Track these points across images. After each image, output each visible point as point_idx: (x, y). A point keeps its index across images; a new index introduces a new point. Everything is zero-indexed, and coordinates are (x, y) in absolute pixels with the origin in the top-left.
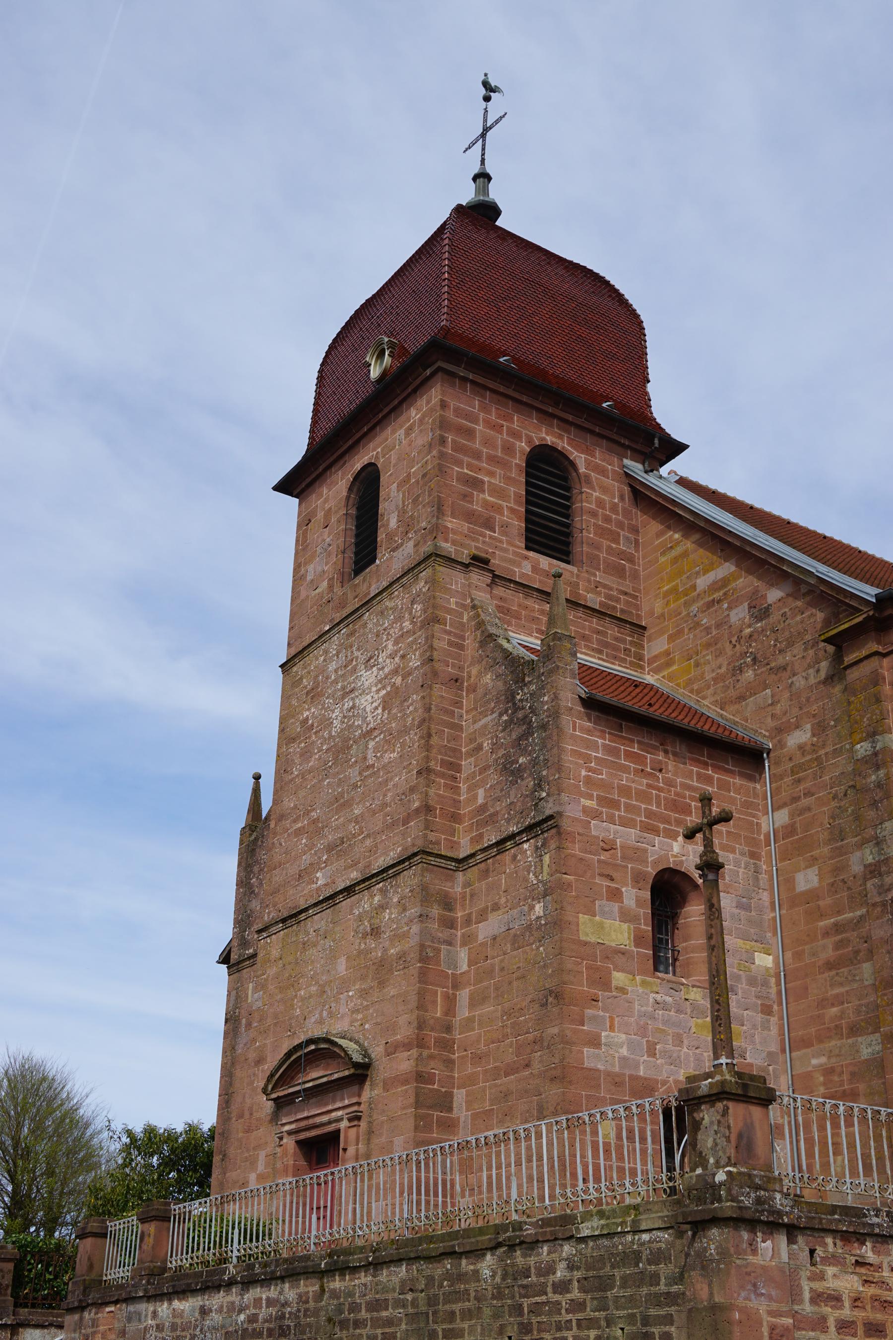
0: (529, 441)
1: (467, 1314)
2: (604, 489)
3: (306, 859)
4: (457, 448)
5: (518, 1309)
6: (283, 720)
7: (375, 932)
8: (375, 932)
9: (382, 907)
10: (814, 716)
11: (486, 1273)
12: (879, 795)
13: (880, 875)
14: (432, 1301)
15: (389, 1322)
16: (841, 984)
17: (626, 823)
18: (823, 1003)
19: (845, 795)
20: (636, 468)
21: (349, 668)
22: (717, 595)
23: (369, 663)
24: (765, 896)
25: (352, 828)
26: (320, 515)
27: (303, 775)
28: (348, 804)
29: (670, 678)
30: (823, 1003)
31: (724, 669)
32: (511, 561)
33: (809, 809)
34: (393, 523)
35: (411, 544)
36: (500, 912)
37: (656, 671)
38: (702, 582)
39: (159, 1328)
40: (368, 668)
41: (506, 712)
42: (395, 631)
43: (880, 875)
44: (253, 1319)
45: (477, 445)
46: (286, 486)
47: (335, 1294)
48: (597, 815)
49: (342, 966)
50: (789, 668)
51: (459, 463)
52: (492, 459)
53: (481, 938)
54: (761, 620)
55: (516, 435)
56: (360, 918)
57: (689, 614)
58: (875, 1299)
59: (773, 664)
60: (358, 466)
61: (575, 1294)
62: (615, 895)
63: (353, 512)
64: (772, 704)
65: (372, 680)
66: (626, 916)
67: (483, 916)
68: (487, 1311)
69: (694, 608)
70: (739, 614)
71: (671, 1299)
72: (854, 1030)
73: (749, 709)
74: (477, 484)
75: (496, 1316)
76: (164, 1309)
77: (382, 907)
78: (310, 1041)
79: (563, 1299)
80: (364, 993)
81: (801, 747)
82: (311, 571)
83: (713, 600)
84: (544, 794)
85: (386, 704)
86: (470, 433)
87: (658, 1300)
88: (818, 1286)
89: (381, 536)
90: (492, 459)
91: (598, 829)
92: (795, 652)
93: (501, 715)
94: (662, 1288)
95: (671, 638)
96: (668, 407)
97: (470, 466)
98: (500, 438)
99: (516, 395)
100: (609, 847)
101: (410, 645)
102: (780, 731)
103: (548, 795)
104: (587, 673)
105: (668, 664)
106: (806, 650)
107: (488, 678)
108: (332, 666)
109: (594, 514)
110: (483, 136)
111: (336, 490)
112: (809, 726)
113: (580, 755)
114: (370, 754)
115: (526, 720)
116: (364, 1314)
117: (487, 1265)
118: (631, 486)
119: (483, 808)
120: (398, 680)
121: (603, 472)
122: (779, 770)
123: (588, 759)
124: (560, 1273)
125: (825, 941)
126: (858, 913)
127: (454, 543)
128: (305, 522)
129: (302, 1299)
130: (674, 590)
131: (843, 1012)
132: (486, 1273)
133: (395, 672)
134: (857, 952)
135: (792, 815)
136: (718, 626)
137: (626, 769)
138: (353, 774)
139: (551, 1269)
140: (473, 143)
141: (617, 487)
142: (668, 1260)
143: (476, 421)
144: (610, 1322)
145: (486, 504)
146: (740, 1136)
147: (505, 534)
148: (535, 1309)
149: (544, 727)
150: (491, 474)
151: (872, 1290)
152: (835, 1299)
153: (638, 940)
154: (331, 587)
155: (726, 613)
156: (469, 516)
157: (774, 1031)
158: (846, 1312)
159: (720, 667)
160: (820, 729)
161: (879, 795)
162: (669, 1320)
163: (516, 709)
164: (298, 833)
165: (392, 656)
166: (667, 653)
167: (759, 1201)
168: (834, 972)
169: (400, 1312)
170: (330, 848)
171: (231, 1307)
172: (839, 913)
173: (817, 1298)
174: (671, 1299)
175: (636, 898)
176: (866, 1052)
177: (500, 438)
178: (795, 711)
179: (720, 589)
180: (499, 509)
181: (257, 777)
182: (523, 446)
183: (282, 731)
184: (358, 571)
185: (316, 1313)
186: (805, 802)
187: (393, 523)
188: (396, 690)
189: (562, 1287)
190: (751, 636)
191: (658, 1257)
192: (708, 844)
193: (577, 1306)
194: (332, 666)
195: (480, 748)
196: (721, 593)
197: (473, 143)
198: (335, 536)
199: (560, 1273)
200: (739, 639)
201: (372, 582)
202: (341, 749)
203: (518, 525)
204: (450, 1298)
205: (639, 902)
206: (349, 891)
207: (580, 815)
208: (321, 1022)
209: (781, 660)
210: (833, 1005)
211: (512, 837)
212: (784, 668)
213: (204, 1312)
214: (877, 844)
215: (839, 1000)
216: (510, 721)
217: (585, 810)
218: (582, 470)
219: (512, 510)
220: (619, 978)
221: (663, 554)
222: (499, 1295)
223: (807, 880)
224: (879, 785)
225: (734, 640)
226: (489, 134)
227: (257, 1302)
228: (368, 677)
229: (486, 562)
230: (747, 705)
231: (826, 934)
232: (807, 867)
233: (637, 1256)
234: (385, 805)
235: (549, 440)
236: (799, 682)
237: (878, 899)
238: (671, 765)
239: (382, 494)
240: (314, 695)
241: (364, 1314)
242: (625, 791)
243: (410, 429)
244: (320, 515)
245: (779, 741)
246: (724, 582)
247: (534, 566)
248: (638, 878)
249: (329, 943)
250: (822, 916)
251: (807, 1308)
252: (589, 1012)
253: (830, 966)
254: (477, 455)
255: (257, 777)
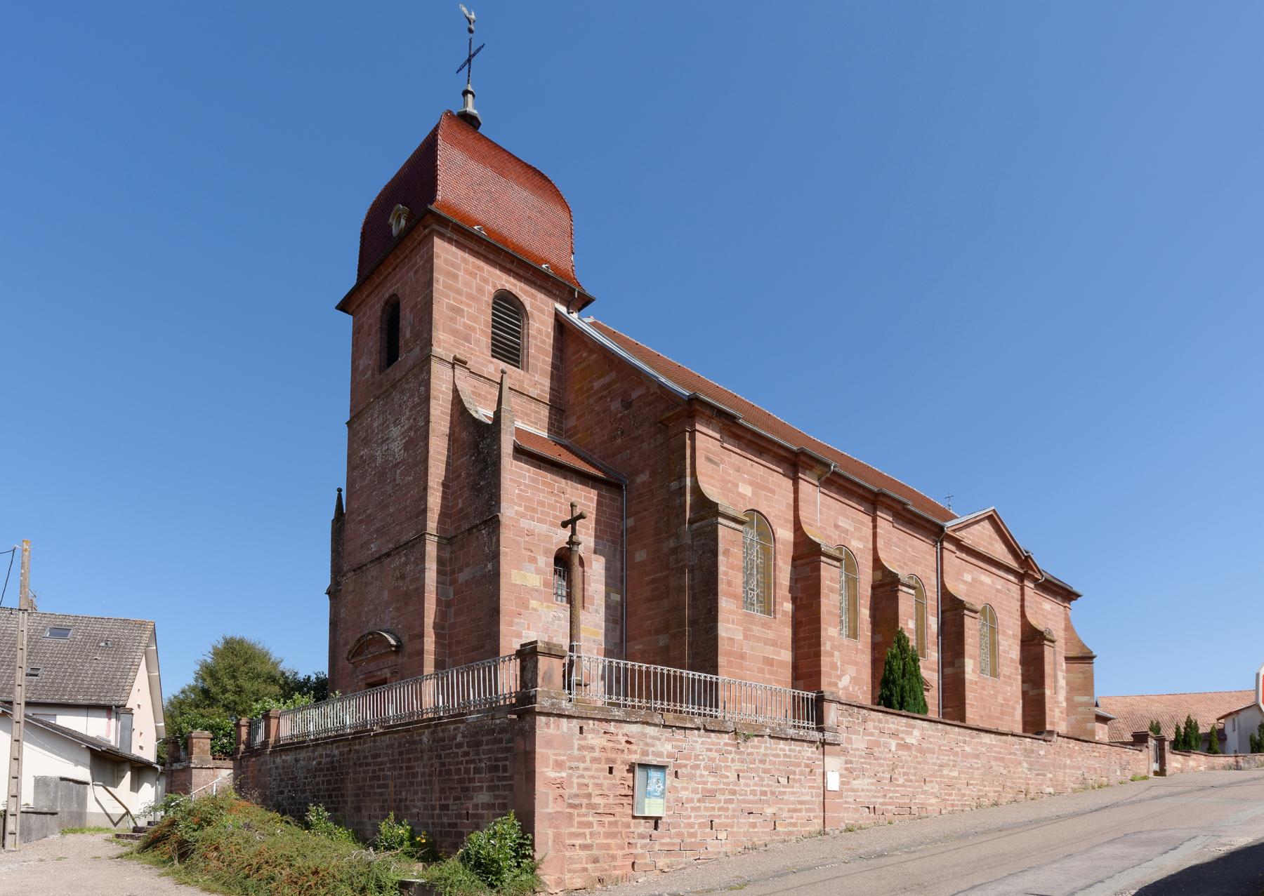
0: (494, 286)
1: (417, 759)
2: (542, 323)
3: (365, 537)
4: (447, 286)
5: (439, 757)
6: (349, 456)
7: (403, 577)
8: (403, 577)
9: (406, 564)
11: (425, 740)
14: (401, 753)
15: (382, 763)
17: (541, 521)
20: (563, 309)
21: (385, 426)
22: (604, 393)
23: (396, 423)
24: (619, 565)
25: (389, 520)
26: (366, 327)
27: (361, 489)
28: (386, 506)
32: (482, 364)
34: (408, 334)
35: (418, 349)
36: (1220, 760)
37: (569, 437)
38: (597, 385)
39: (277, 768)
40: (396, 425)
42: (410, 404)
44: (319, 763)
45: (460, 285)
46: (343, 306)
47: (357, 751)
48: (524, 516)
49: (386, 596)
51: (448, 297)
52: (469, 296)
53: (460, 580)
55: (485, 280)
56: (394, 569)
58: (613, 748)
60: (387, 296)
61: (465, 749)
62: (533, 560)
63: (385, 326)
65: (398, 433)
66: (538, 571)
67: (461, 570)
68: (425, 757)
69: (591, 401)
70: (616, 405)
71: (508, 750)
72: (657, 632)
74: (459, 311)
75: (430, 759)
76: (278, 760)
77: (406, 564)
78: (371, 633)
79: (460, 751)
80: (397, 610)
81: (643, 483)
82: (362, 364)
85: (406, 447)
86: (455, 277)
87: (502, 750)
88: (582, 743)
89: (402, 342)
90: (469, 296)
91: (525, 524)
94: (504, 745)
95: (578, 418)
97: (454, 300)
98: (476, 282)
99: (485, 253)
100: (530, 533)
101: (418, 412)
104: (519, 432)
107: (464, 435)
108: (376, 424)
109: (535, 338)
110: (469, 61)
111: (374, 310)
113: (514, 481)
114: (398, 477)
115: (485, 460)
116: (370, 760)
119: (461, 510)
121: (542, 311)
123: (519, 484)
124: (459, 739)
127: (444, 348)
128: (357, 331)
129: (342, 754)
132: (425, 740)
133: (410, 429)
136: (604, 411)
137: (543, 491)
138: (389, 488)
139: (454, 738)
140: (463, 67)
141: (551, 321)
142: (507, 732)
143: (459, 269)
144: (480, 761)
145: (465, 325)
146: (545, 673)
147: (477, 345)
148: (447, 756)
150: (469, 306)
151: (611, 744)
152: (592, 748)
153: (546, 584)
154: (373, 374)
156: (455, 333)
157: (618, 632)
158: (596, 754)
160: (654, 474)
162: (506, 759)
163: (479, 453)
164: (360, 522)
165: (408, 419)
166: (575, 427)
167: (553, 704)
169: (386, 759)
170: (377, 531)
171: (309, 759)
173: (581, 748)
174: (508, 750)
175: (546, 562)
176: (662, 643)
177: (476, 282)
180: (474, 330)
181: (340, 490)
182: (490, 291)
183: (349, 463)
184: (389, 365)
185: (348, 760)
187: (408, 334)
188: (411, 440)
189: (459, 746)
192: (574, 532)
193: (466, 754)
194: (376, 424)
195: (460, 476)
197: (463, 67)
198: (373, 343)
199: (459, 739)
201: (396, 372)
202: (382, 474)
203: (486, 341)
204: (408, 752)
205: (547, 565)
206: (388, 555)
207: (513, 515)
208: (376, 624)
211: (476, 526)
213: (297, 760)
216: (476, 461)
217: (517, 512)
218: (528, 308)
219: (483, 331)
220: (533, 603)
222: (431, 750)
226: (473, 60)
227: (321, 756)
228: (395, 431)
229: (465, 363)
231: (648, 584)
233: (493, 731)
234: (406, 507)
235: (508, 287)
236: (645, 446)
238: (569, 490)
239: (401, 314)
240: (366, 442)
241: (370, 760)
242: (542, 503)
243: (416, 272)
244: (366, 327)
246: (609, 385)
247: (494, 367)
248: (546, 552)
249: (378, 583)
251: (576, 752)
252: (516, 620)
254: (459, 292)
255: (340, 490)
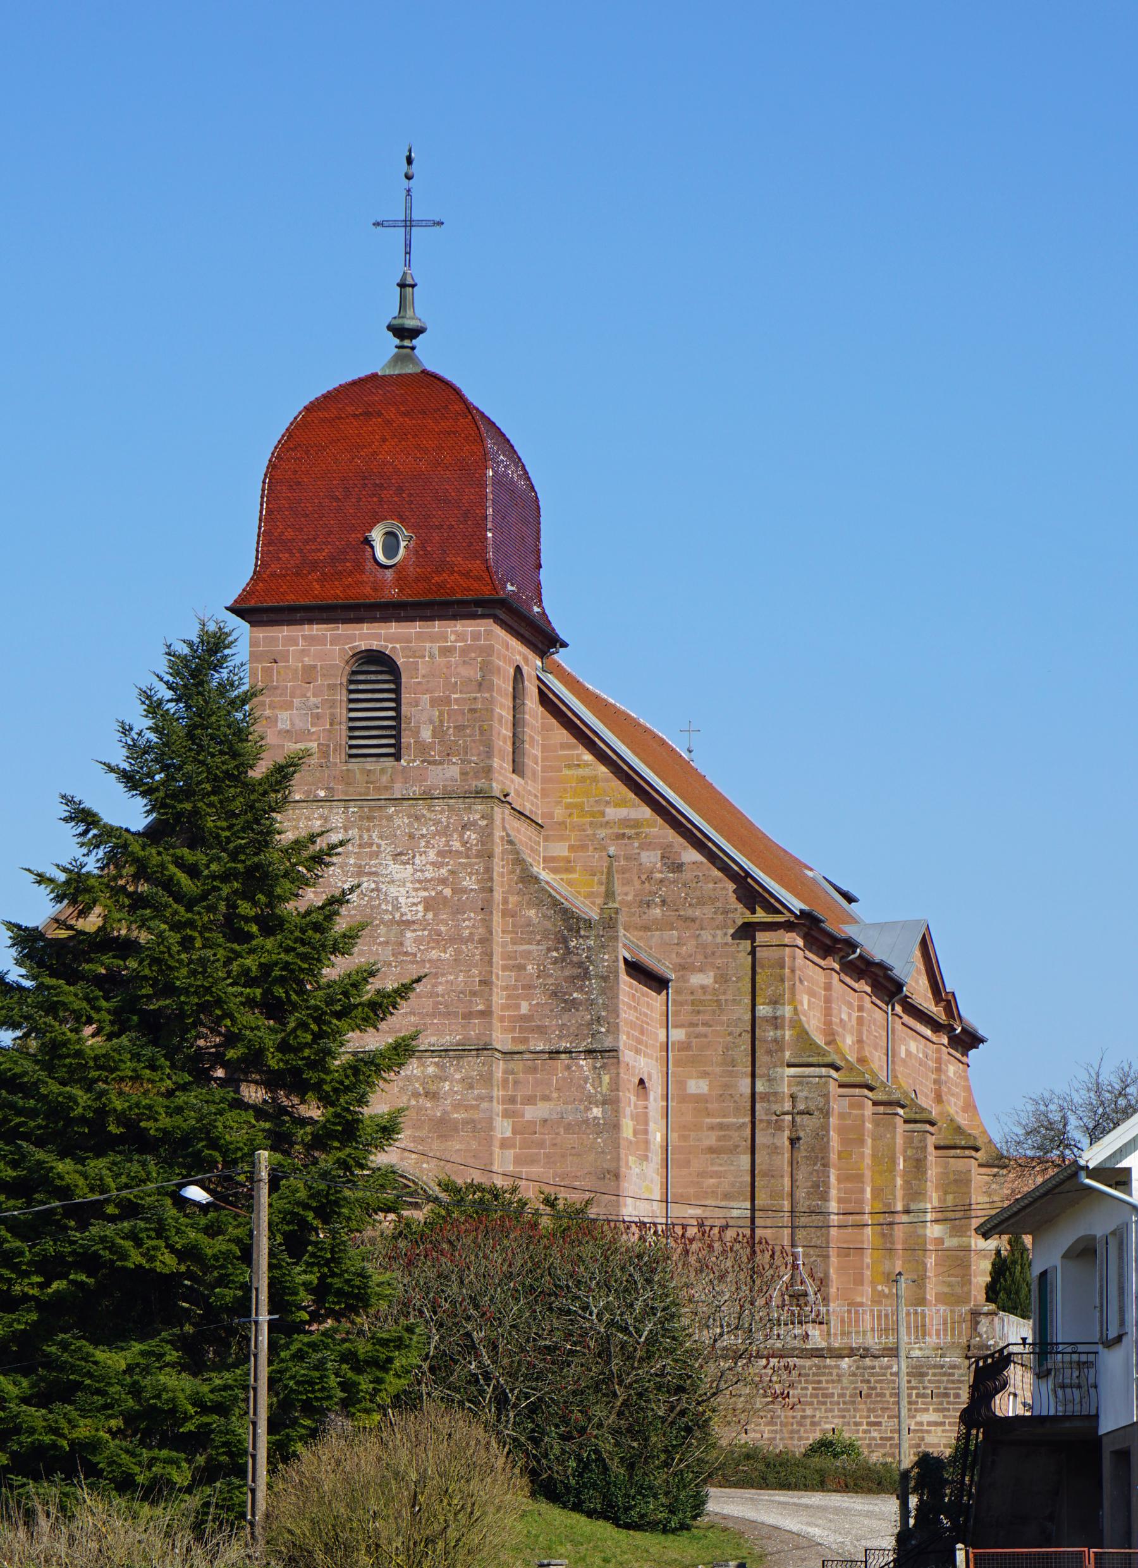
5: (868, 1382)
10: (718, 968)
12: (773, 1047)
13: (769, 1101)
16: (721, 1165)
18: (702, 1174)
19: (740, 1035)
29: (570, 883)
30: (702, 1174)
31: (630, 898)
33: (706, 1036)
37: (554, 871)
41: (557, 950)
43: (769, 1101)
50: (698, 922)
54: (674, 872)
57: (594, 835)
59: (682, 913)
64: (677, 944)
70: (650, 858)
73: (654, 940)
83: (624, 834)
84: (603, 1030)
92: (706, 911)
93: (549, 950)
96: (557, 607)
102: (684, 968)
103: (608, 1031)
105: (568, 870)
106: (715, 913)
112: (712, 974)
117: (845, 1363)
118: (539, 688)
120: (448, 892)
122: (680, 998)
125: (710, 1133)
126: (741, 1120)
130: (580, 806)
131: (720, 1183)
134: (737, 1146)
135: (688, 1035)
149: (605, 979)
155: (637, 851)
159: (626, 894)
161: (773, 1047)
168: (715, 1156)
172: (724, 1116)
178: (700, 957)
179: (632, 827)
186: (701, 1029)
187: (426, 734)
190: (661, 881)
191: (954, 1367)
196: (633, 831)
200: (649, 879)
209: (690, 912)
210: (711, 1177)
212: (693, 920)
214: (769, 1080)
215: (718, 1175)
221: (569, 766)
223: (697, 1086)
224: (775, 1041)
225: (644, 877)
230: (652, 936)
231: (712, 1128)
232: (698, 1077)
233: (942, 1367)
237: (764, 1118)
245: (682, 976)
250: (708, 1115)
253: (711, 1150)
